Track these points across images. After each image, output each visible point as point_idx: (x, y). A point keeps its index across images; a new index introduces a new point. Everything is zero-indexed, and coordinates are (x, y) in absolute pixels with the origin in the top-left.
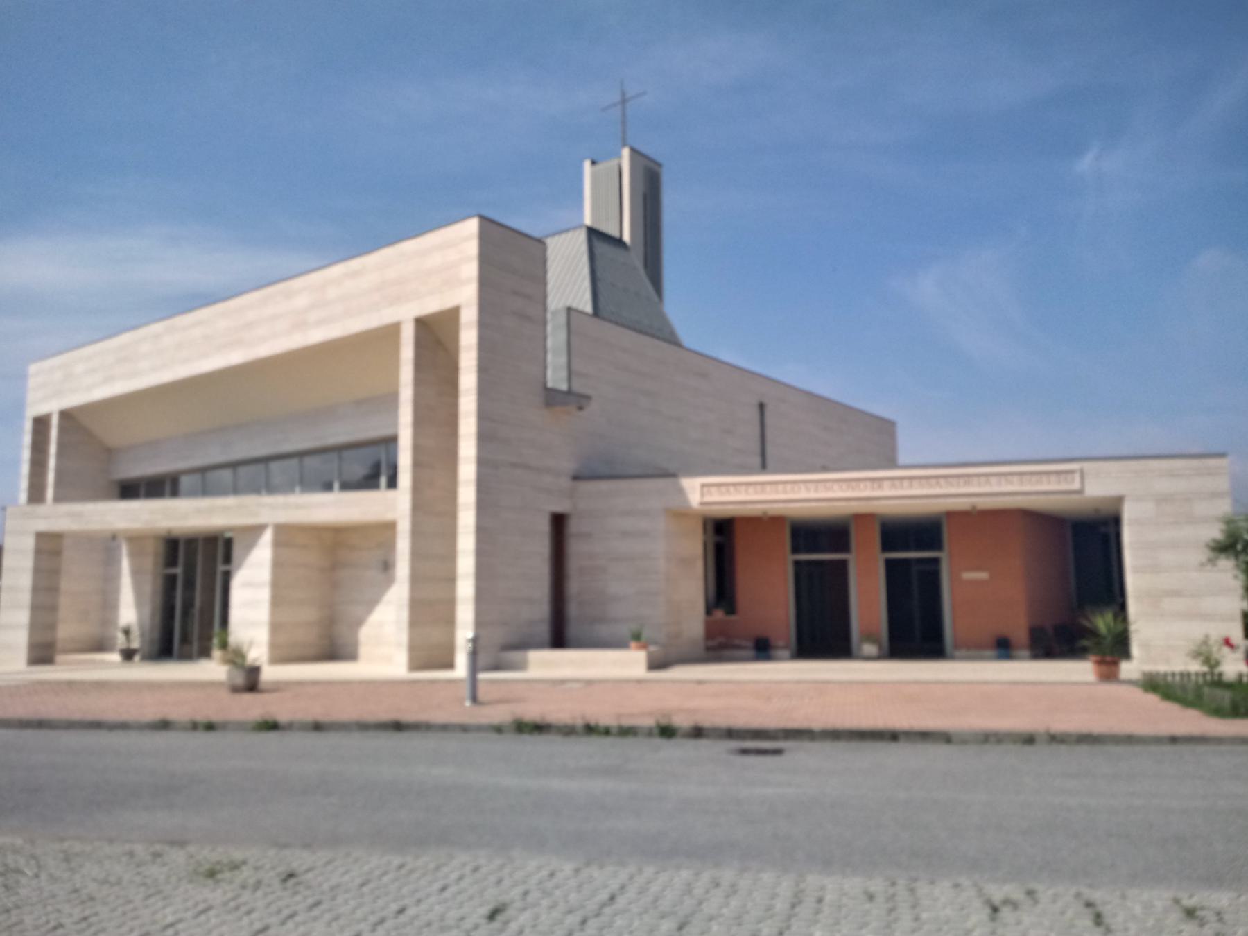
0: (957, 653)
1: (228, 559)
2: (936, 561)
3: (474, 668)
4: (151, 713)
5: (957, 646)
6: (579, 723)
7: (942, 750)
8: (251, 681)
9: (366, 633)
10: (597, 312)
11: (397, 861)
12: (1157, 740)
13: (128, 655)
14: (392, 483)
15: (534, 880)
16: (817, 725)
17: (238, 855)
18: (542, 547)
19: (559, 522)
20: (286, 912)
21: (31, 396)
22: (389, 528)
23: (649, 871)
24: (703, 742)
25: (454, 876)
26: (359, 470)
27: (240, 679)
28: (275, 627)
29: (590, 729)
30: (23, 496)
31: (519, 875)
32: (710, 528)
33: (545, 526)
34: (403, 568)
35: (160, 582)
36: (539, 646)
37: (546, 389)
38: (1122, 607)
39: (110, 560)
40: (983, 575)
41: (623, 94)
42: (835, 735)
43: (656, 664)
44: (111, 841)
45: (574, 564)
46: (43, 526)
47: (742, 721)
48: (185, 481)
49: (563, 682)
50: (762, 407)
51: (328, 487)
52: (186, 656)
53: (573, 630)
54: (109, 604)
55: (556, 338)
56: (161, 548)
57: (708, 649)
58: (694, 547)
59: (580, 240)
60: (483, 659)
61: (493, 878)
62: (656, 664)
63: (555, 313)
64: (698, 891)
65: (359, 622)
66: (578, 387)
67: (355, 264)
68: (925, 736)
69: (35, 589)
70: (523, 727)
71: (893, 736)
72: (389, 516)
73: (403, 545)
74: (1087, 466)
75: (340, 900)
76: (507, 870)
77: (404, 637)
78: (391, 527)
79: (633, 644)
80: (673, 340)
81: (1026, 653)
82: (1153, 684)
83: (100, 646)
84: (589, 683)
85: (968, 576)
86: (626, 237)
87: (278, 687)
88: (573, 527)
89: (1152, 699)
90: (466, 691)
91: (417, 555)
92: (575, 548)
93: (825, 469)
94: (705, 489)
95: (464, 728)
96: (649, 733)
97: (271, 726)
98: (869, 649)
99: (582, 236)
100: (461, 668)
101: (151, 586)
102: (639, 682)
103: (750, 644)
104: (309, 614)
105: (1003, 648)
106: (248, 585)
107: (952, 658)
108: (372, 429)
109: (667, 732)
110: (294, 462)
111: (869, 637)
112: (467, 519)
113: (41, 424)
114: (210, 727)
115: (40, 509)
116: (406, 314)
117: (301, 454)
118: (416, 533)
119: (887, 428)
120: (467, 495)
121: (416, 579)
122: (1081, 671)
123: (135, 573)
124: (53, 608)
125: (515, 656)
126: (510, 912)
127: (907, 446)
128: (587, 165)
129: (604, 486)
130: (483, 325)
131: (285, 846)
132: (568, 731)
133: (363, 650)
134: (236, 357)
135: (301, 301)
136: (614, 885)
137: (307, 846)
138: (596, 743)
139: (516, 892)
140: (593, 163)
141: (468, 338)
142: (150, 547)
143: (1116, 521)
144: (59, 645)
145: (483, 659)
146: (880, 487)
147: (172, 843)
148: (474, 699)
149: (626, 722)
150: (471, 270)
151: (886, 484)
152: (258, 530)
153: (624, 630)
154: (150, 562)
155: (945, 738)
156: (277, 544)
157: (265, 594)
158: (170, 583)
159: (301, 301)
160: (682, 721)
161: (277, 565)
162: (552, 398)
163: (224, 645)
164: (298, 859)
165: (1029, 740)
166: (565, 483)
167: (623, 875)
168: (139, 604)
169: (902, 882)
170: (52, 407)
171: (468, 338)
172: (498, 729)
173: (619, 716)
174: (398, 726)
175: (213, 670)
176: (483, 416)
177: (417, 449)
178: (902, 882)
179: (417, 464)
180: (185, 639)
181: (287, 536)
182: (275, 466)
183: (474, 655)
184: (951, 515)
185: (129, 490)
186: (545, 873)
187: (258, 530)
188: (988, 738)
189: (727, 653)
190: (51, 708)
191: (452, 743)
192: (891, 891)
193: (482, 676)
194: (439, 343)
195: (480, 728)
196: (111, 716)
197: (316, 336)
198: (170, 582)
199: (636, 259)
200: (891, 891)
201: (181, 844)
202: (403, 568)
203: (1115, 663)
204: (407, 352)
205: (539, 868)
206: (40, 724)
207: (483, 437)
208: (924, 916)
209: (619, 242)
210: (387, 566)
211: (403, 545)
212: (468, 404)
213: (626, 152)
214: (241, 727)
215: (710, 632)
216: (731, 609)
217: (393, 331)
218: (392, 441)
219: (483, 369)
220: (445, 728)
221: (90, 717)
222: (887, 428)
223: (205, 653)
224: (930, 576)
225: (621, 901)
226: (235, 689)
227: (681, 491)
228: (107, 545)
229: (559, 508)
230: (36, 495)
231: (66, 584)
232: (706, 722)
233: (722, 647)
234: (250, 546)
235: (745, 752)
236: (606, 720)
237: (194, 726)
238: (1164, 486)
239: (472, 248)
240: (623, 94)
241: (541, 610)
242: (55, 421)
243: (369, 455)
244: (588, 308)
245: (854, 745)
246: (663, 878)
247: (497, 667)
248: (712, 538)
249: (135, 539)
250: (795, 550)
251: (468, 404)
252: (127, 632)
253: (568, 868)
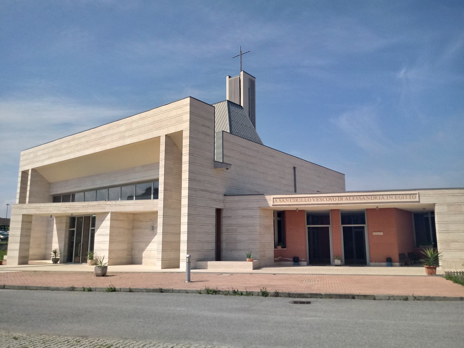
0: (371, 264)
1: (93, 225)
2: (363, 228)
4: (68, 284)
5: (371, 261)
6: (231, 290)
8: (103, 273)
10: (231, 132)
12: (455, 299)
13: (55, 261)
14: (156, 197)
16: (323, 292)
19: (219, 212)
21: (21, 164)
26: (141, 191)
27: (99, 272)
28: (111, 251)
29: (235, 293)
30: (17, 201)
32: (276, 215)
33: (214, 213)
34: (160, 229)
35: (68, 233)
37: (214, 161)
38: (435, 246)
39: (49, 225)
40: (382, 234)
41: (241, 52)
42: (330, 296)
43: (256, 267)
44: (59, 336)
45: (224, 228)
46: (25, 212)
48: (77, 196)
49: (222, 274)
50: (294, 168)
52: (77, 262)
53: (224, 253)
54: (48, 242)
55: (218, 142)
56: (68, 221)
57: (275, 261)
58: (270, 222)
62: (256, 267)
63: (217, 133)
65: (143, 250)
66: (225, 161)
67: (143, 115)
68: (365, 297)
69: (22, 236)
71: (353, 297)
72: (155, 209)
73: (160, 220)
74: (420, 191)
77: (160, 256)
78: (156, 213)
79: (247, 259)
81: (398, 264)
82: (449, 276)
83: (45, 258)
84: (232, 274)
85: (374, 234)
86: (242, 105)
87: (113, 275)
88: (224, 214)
89: (450, 282)
90: (186, 278)
92: (225, 222)
93: (318, 192)
95: (187, 292)
97: (113, 290)
98: (337, 262)
99: (226, 103)
100: (183, 267)
102: (251, 274)
103: (292, 259)
104: (124, 246)
105: (389, 262)
106: (99, 235)
107: (370, 266)
109: (265, 294)
111: (338, 257)
112: (184, 211)
113: (25, 173)
114: (90, 290)
115: (24, 206)
116: (162, 133)
117: (121, 186)
118: (165, 216)
122: (421, 271)
123: (58, 230)
124: (28, 243)
127: (350, 183)
129: (236, 198)
131: (126, 339)
132: (227, 293)
134: (98, 149)
135: (123, 128)
137: (134, 339)
140: (230, 77)
141: (186, 142)
142: (64, 220)
143: (433, 213)
144: (30, 257)
145: (192, 265)
146: (375, 198)
147: (83, 337)
148: (189, 281)
150: (187, 117)
153: (244, 254)
154: (64, 226)
155: (374, 298)
156: (112, 219)
157: (107, 238)
158: (71, 234)
159: (123, 128)
160: (270, 290)
161: (111, 227)
162: (217, 165)
163: (92, 258)
165: (406, 299)
166: (221, 197)
168: (59, 242)
170: (29, 167)
171: (186, 142)
173: (246, 288)
174: (161, 291)
175: (88, 267)
176: (191, 172)
177: (165, 184)
180: (77, 255)
181: (116, 216)
183: (189, 263)
184: (369, 210)
185: (56, 199)
187: (107, 213)
188: (390, 298)
189: (282, 263)
190: (29, 282)
191: (182, 298)
193: (192, 271)
195: (193, 292)
196: (52, 285)
197: (128, 141)
198: (72, 233)
201: (86, 337)
202: (160, 229)
203: (435, 268)
204: (162, 148)
206: (26, 288)
207: (191, 180)
210: (154, 228)
211: (160, 220)
212: (185, 167)
213: (242, 73)
214: (101, 290)
215: (276, 254)
218: (157, 180)
220: (179, 291)
223: (84, 261)
224: (360, 234)
226: (97, 275)
227: (266, 200)
230: (22, 201)
233: (280, 260)
235: (295, 302)
236: (241, 289)
237: (84, 290)
238: (450, 200)
239: (188, 109)
240: (241, 52)
241: (212, 246)
242: (30, 172)
244: (229, 131)
245: (328, 300)
247: (195, 268)
248: (277, 219)
249: (58, 217)
250: (343, 223)
251: (185, 167)
252: (55, 252)
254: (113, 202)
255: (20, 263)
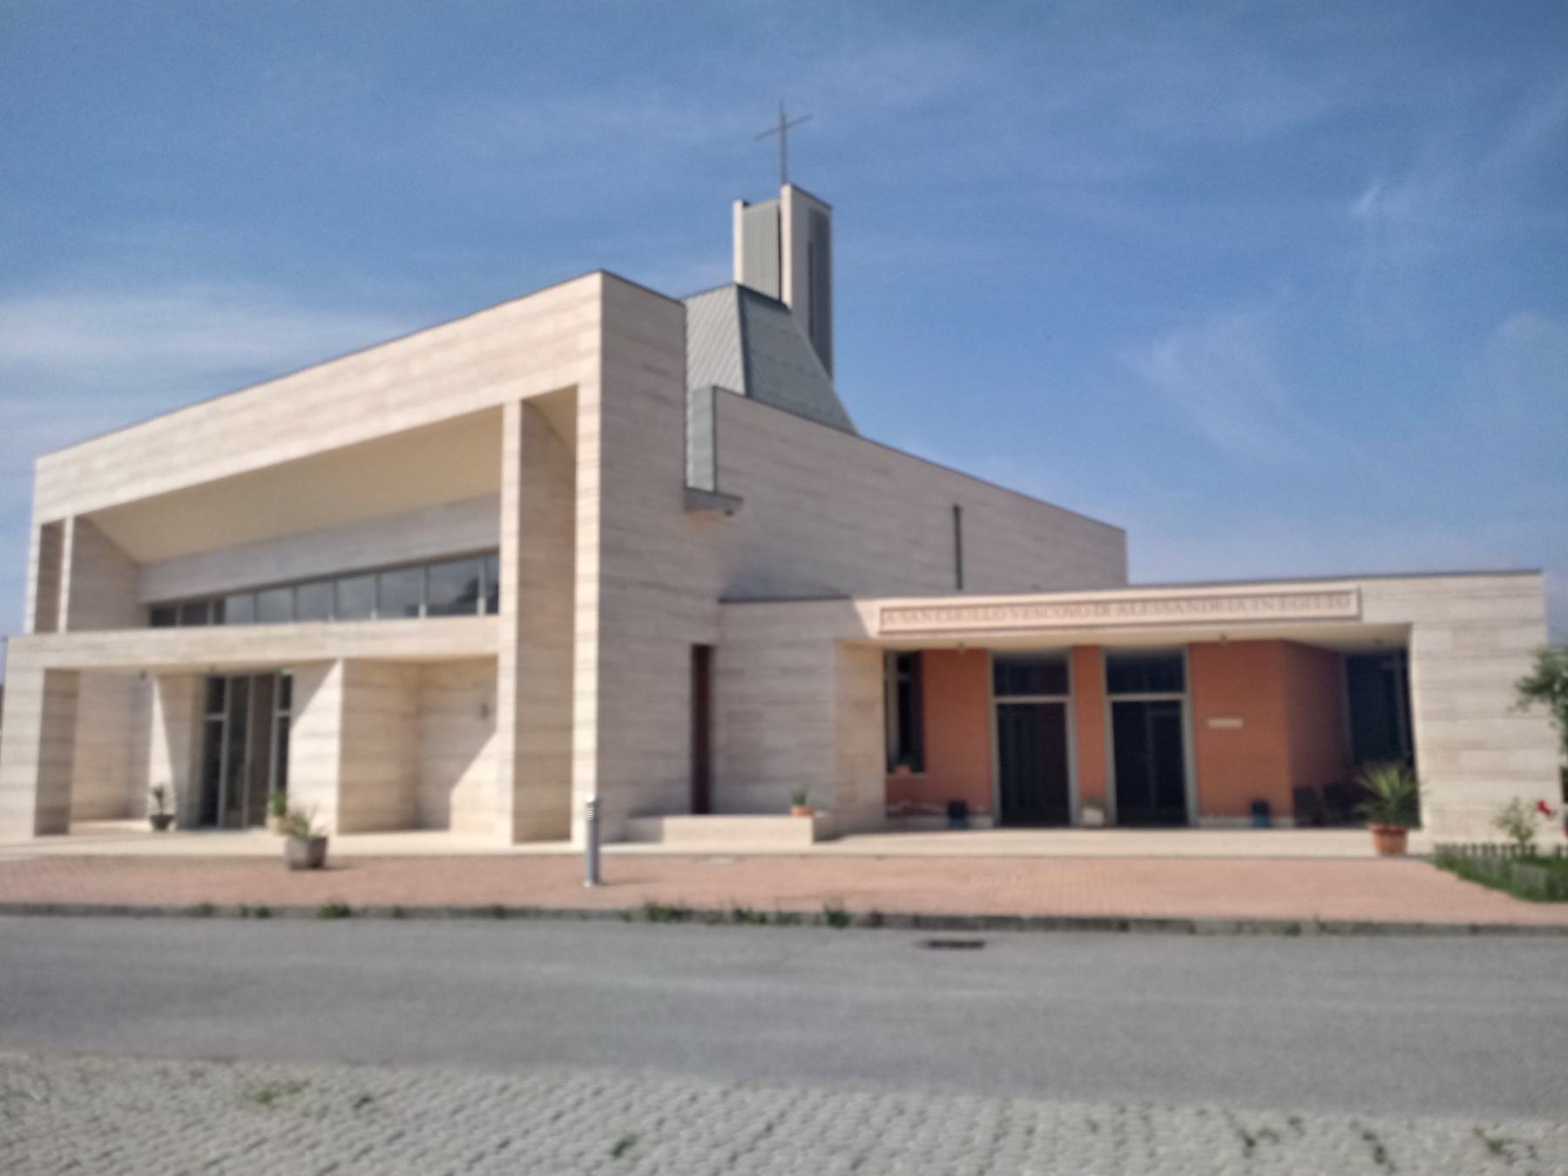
0: (1203, 821)
1: (286, 702)
2: (1176, 705)
3: (596, 840)
4: (190, 895)
5: (1202, 812)
6: (728, 908)
7: (1184, 942)
8: (315, 856)
9: (459, 796)
10: (749, 392)
11: (498, 1082)
12: (1454, 930)
13: (161, 823)
14: (493, 607)
15: (671, 1106)
16: (1026, 910)
17: (299, 1075)
18: (681, 687)
19: (702, 656)
20: (359, 1146)
21: (39, 498)
22: (489, 663)
23: (815, 1094)
24: (883, 933)
25: (570, 1101)
26: (451, 591)
27: (301, 854)
28: (346, 788)
29: (742, 917)
30: (29, 624)
31: (652, 1099)
32: (892, 663)
33: (684, 661)
34: (506, 713)
35: (201, 731)
36: (677, 811)
37: (686, 489)
38: (1410, 762)
39: (139, 704)
40: (1235, 723)
41: (783, 118)
42: (1049, 923)
43: (824, 835)
44: (139, 1057)
45: (721, 709)
46: (54, 661)
47: (932, 905)
48: (232, 605)
49: (707, 856)
50: (957, 511)
51: (412, 612)
52: (234, 825)
53: (719, 792)
54: (137, 759)
55: (698, 424)
56: (202, 689)
57: (890, 815)
58: (872, 687)
59: (728, 301)
60: (606, 828)
61: (619, 1104)
62: (824, 835)
63: (697, 393)
64: (877, 1119)
65: (452, 782)
66: (726, 486)
67: (446, 331)
68: (1162, 925)
69: (45, 741)
70: (657, 914)
71: (1122, 925)
72: (488, 649)
73: (506, 685)
74: (1366, 585)
75: (427, 1130)
76: (636, 1094)
77: (507, 800)
78: (491, 662)
79: (795, 809)
80: (846, 428)
81: (1289, 820)
82: (1449, 859)
83: (126, 811)
84: (741, 858)
85: (1216, 723)
86: (787, 298)
87: (349, 863)
88: (720, 662)
89: (1448, 878)
90: (585, 868)
91: (523, 697)
92: (723, 688)
93: (1036, 589)
94: (886, 615)
95: (583, 915)
96: (816, 921)
97: (341, 912)
98: (1092, 815)
99: (731, 297)
100: (579, 840)
101: (190, 736)
102: (803, 856)
103: (942, 809)
104: (389, 771)
105: (1261, 814)
106: (312, 735)
107: (1196, 826)
108: (467, 539)
109: (838, 919)
110: (369, 581)
111: (1092, 801)
112: (586, 652)
113: (51, 532)
114: (264, 913)
115: (51, 640)
116: (510, 394)
117: (378, 571)
118: (522, 669)
119: (1114, 538)
120: (587, 621)
121: (523, 728)
122: (1358, 843)
123: (170, 720)
124: (67, 764)
125: (647, 824)
126: (641, 1146)
127: (1140, 561)
128: (738, 207)
129: (758, 610)
130: (607, 408)
131: (358, 1063)
132: (714, 918)
133: (456, 817)
134: (296, 449)
135: (378, 378)
136: (772, 1112)
137: (385, 1063)
138: (748, 933)
139: (649, 1121)
140: (746, 204)
141: (589, 425)
142: (189, 687)
143: (1402, 654)
144: (75, 811)
145: (606, 828)
146: (1106, 612)
147: (217, 1059)
148: (596, 878)
149: (787, 907)
150: (592, 339)
151: (1114, 608)
152: (324, 666)
153: (784, 792)
154: (188, 707)
155: (1188, 927)
156: (349, 683)
157: (333, 747)
158: (213, 733)
159: (378, 378)
160: (857, 906)
161: (348, 709)
162: (693, 500)
163: (282, 811)
164: (375, 1079)
165: (1293, 929)
166: (710, 606)
167: (783, 1100)
168: (174, 758)
169: (1133, 1108)
170: (65, 511)
171: (589, 425)
172: (626, 916)
173: (778, 899)
174: (500, 913)
175: (267, 841)
176: (607, 522)
177: (524, 564)
178: (1133, 1108)
179: (524, 584)
180: (233, 803)
181: (360, 673)
182: (345, 586)
183: (595, 823)
184: (1195, 647)
185: (162, 616)
186: (684, 1096)
187: (324, 666)
188: (1241, 927)
189: (913, 820)
190: (64, 890)
191: (567, 934)
192: (1119, 1119)
193: (606, 849)
194: (551, 431)
195: (603, 915)
196: (139, 899)
197: (397, 422)
198: (214, 731)
199: (799, 325)
200: (1119, 1119)
201: (228, 1060)
202: (506, 713)
203: (1401, 834)
204: (512, 443)
205: (678, 1091)
206: (51, 910)
207: (607, 550)
208: (1162, 1150)
209: (777, 304)
210: (487, 711)
211: (506, 685)
212: (588, 507)
213: (786, 192)
214: (303, 913)
215: (892, 794)
216: (918, 765)
217: (493, 416)
218: (492, 553)
219: (607, 464)
220: (558, 914)
221: (112, 901)
222: (1114, 538)
223: (258, 820)
224: (1169, 724)
225: (780, 1133)
226: (296, 866)
227: (855, 617)
228: (134, 684)
229: (703, 638)
230: (45, 621)
231: (83, 734)
232: (887, 907)
233: (907, 812)
234: (314, 686)
235: (936, 945)
236: (761, 905)
237: (244, 912)
238: (1462, 610)
239: (594, 311)
240: (783, 118)
241: (680, 766)
242: (69, 529)
243: (463, 571)
244: (739, 387)
245: (1073, 936)
246: (833, 1103)
247: (624, 838)
248: (895, 676)
249: (169, 678)
250: (999, 691)
251: (588, 507)
252: (159, 794)
253: (714, 1091)
254: (350, 627)
255: (524, 833)
